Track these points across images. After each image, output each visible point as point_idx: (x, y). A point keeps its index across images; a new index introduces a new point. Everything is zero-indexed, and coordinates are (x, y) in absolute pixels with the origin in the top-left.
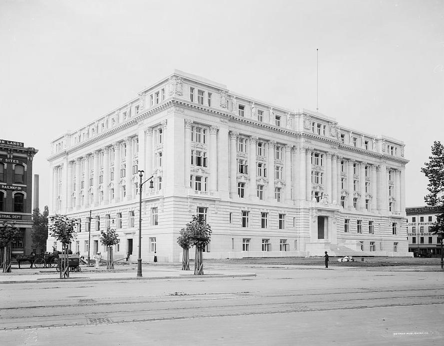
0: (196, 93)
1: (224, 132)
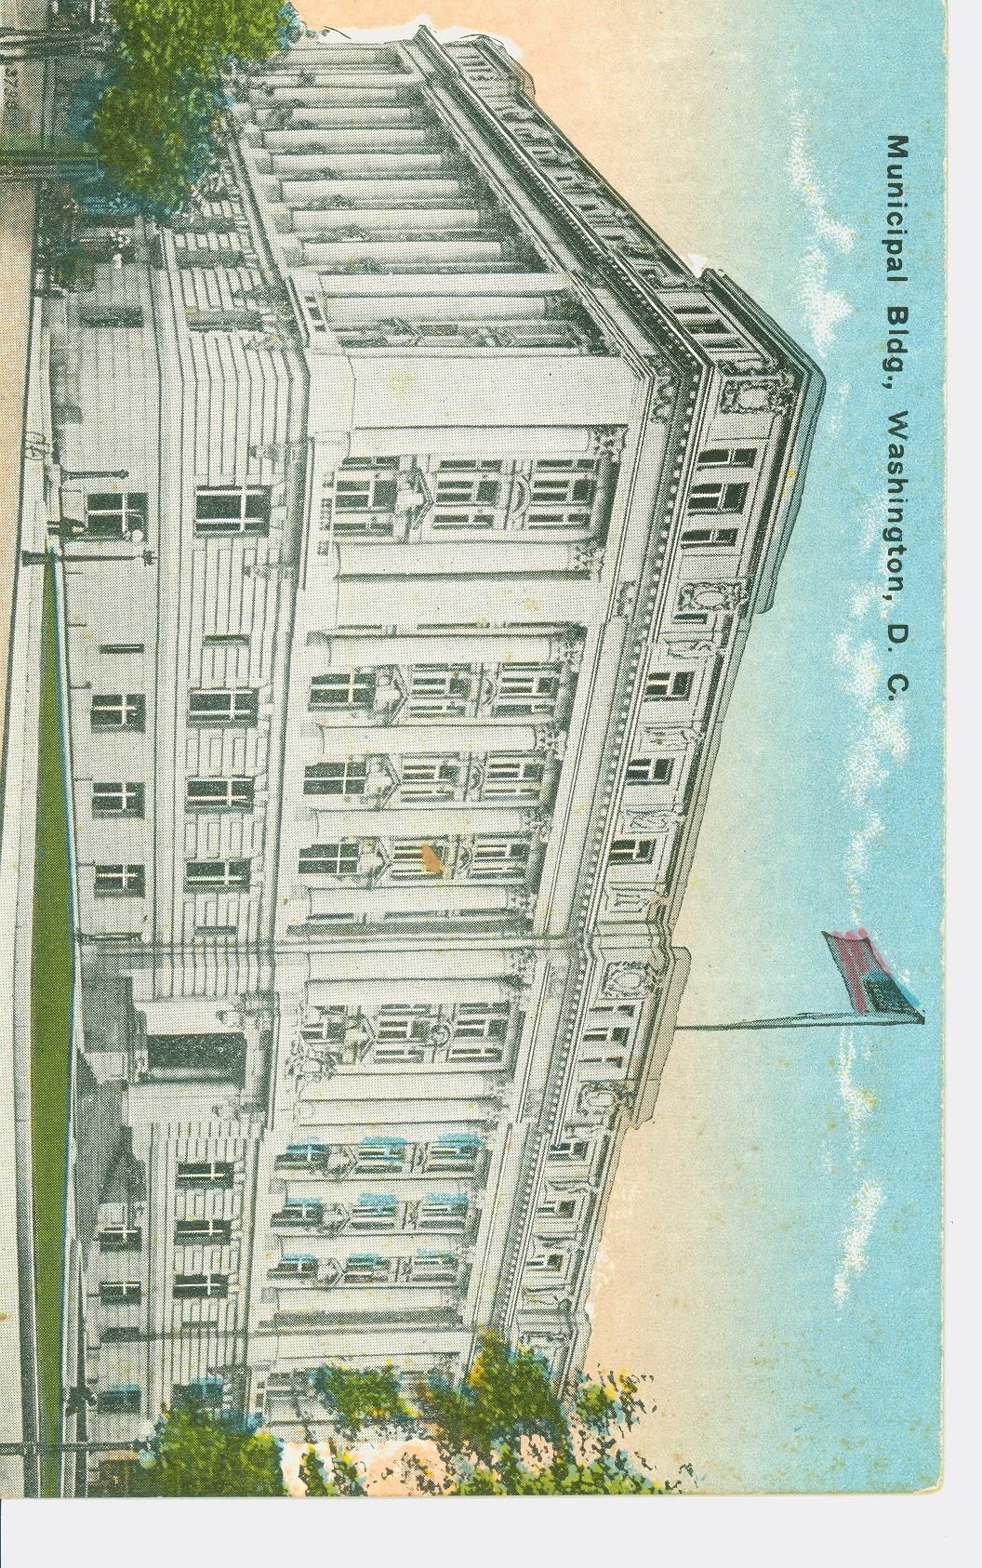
0: (726, 476)
1: (585, 603)
